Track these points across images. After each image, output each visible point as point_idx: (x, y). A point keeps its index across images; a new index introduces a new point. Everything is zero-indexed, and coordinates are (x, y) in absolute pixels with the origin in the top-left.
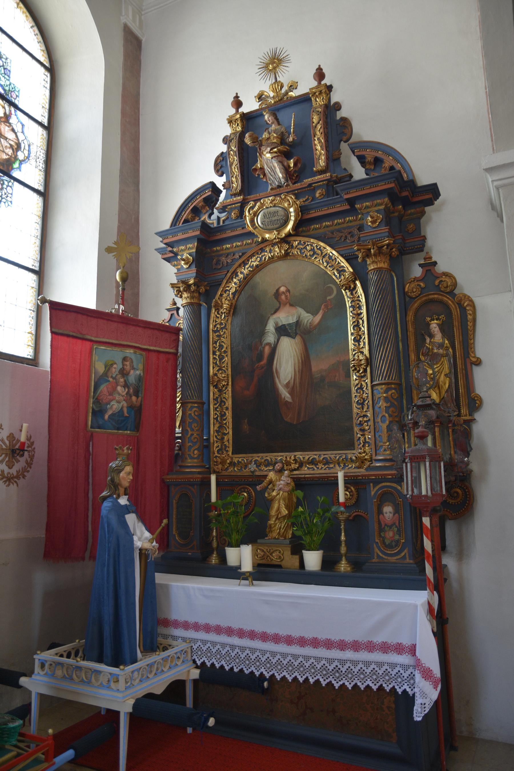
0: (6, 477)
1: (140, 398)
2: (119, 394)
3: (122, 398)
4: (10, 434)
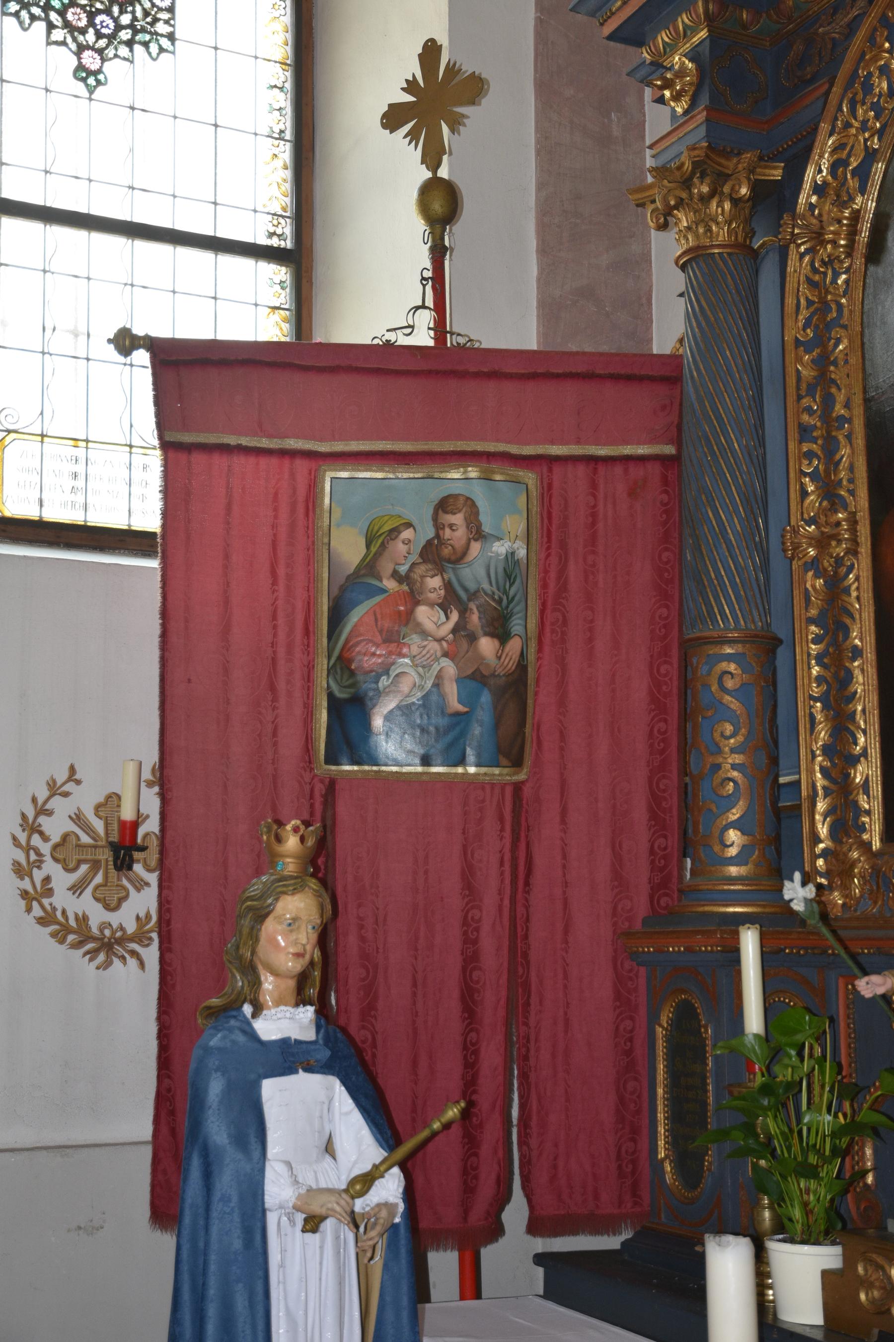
0: (94, 939)
1: (514, 646)
2: (425, 634)
3: (434, 647)
4: (109, 797)
